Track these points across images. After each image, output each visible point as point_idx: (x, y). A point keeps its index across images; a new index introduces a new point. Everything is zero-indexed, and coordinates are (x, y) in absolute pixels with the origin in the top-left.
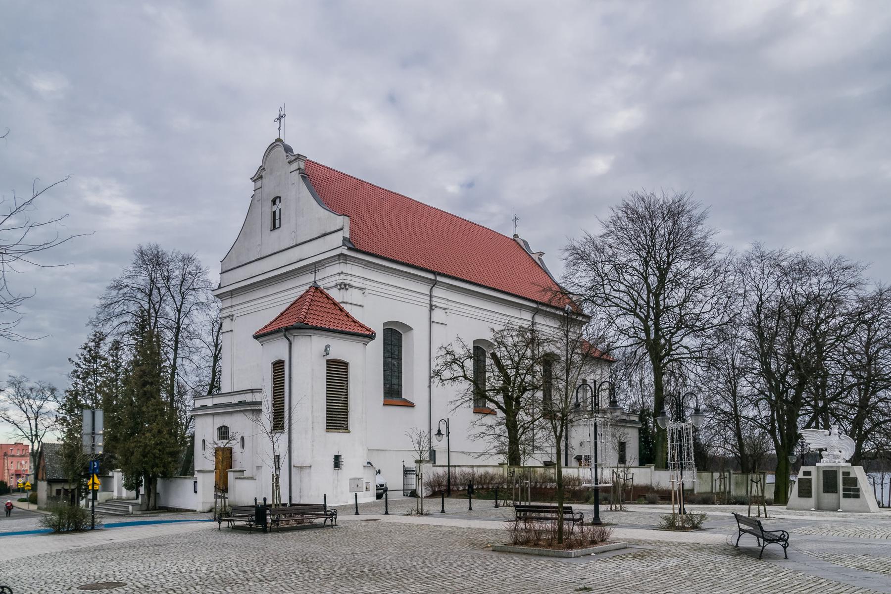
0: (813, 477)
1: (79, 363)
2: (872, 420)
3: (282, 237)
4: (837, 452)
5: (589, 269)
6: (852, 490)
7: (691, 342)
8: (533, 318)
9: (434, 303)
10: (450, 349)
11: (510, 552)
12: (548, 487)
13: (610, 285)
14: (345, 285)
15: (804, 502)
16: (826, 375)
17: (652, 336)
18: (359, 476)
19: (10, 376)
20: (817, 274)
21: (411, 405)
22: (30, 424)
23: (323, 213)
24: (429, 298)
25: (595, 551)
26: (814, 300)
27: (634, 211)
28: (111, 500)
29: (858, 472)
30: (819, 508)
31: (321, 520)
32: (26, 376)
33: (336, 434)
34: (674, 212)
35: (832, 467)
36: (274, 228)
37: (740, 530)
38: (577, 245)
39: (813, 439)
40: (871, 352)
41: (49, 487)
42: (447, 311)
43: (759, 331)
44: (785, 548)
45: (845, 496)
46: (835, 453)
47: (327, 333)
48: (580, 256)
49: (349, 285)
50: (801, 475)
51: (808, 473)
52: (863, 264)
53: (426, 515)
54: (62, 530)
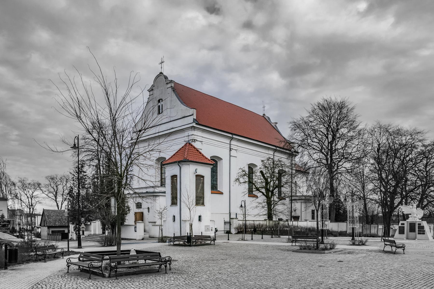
0: (405, 226)
1: (74, 174)
2: (427, 200)
3: (164, 118)
4: (415, 215)
5: (301, 132)
6: (422, 230)
7: (348, 165)
8: (274, 154)
9: (231, 148)
10: (244, 169)
11: (300, 252)
12: (285, 230)
13: (311, 139)
14: (194, 140)
15: (401, 236)
16: (407, 180)
17: (329, 163)
18: (208, 225)
19: (19, 178)
20: (405, 135)
21: (222, 193)
22: (29, 200)
23: (183, 107)
24: (229, 145)
25: (333, 251)
26: (403, 146)
27: (323, 106)
28: (91, 235)
29: (424, 223)
30: (407, 238)
31: (209, 242)
32: (26, 177)
33: (199, 206)
34: (341, 106)
35: (413, 221)
36: (159, 113)
37: (385, 244)
38: (295, 121)
39: (405, 209)
40: (428, 169)
41: (48, 230)
42: (237, 151)
43: (378, 160)
44: (404, 250)
45: (419, 233)
46: (415, 216)
47: (196, 164)
48: (297, 126)
49: (196, 140)
50: (400, 225)
51: (403, 224)
52: (426, 131)
53: (246, 240)
54: (113, 244)
